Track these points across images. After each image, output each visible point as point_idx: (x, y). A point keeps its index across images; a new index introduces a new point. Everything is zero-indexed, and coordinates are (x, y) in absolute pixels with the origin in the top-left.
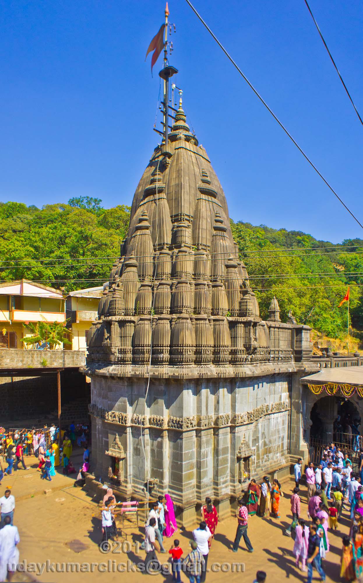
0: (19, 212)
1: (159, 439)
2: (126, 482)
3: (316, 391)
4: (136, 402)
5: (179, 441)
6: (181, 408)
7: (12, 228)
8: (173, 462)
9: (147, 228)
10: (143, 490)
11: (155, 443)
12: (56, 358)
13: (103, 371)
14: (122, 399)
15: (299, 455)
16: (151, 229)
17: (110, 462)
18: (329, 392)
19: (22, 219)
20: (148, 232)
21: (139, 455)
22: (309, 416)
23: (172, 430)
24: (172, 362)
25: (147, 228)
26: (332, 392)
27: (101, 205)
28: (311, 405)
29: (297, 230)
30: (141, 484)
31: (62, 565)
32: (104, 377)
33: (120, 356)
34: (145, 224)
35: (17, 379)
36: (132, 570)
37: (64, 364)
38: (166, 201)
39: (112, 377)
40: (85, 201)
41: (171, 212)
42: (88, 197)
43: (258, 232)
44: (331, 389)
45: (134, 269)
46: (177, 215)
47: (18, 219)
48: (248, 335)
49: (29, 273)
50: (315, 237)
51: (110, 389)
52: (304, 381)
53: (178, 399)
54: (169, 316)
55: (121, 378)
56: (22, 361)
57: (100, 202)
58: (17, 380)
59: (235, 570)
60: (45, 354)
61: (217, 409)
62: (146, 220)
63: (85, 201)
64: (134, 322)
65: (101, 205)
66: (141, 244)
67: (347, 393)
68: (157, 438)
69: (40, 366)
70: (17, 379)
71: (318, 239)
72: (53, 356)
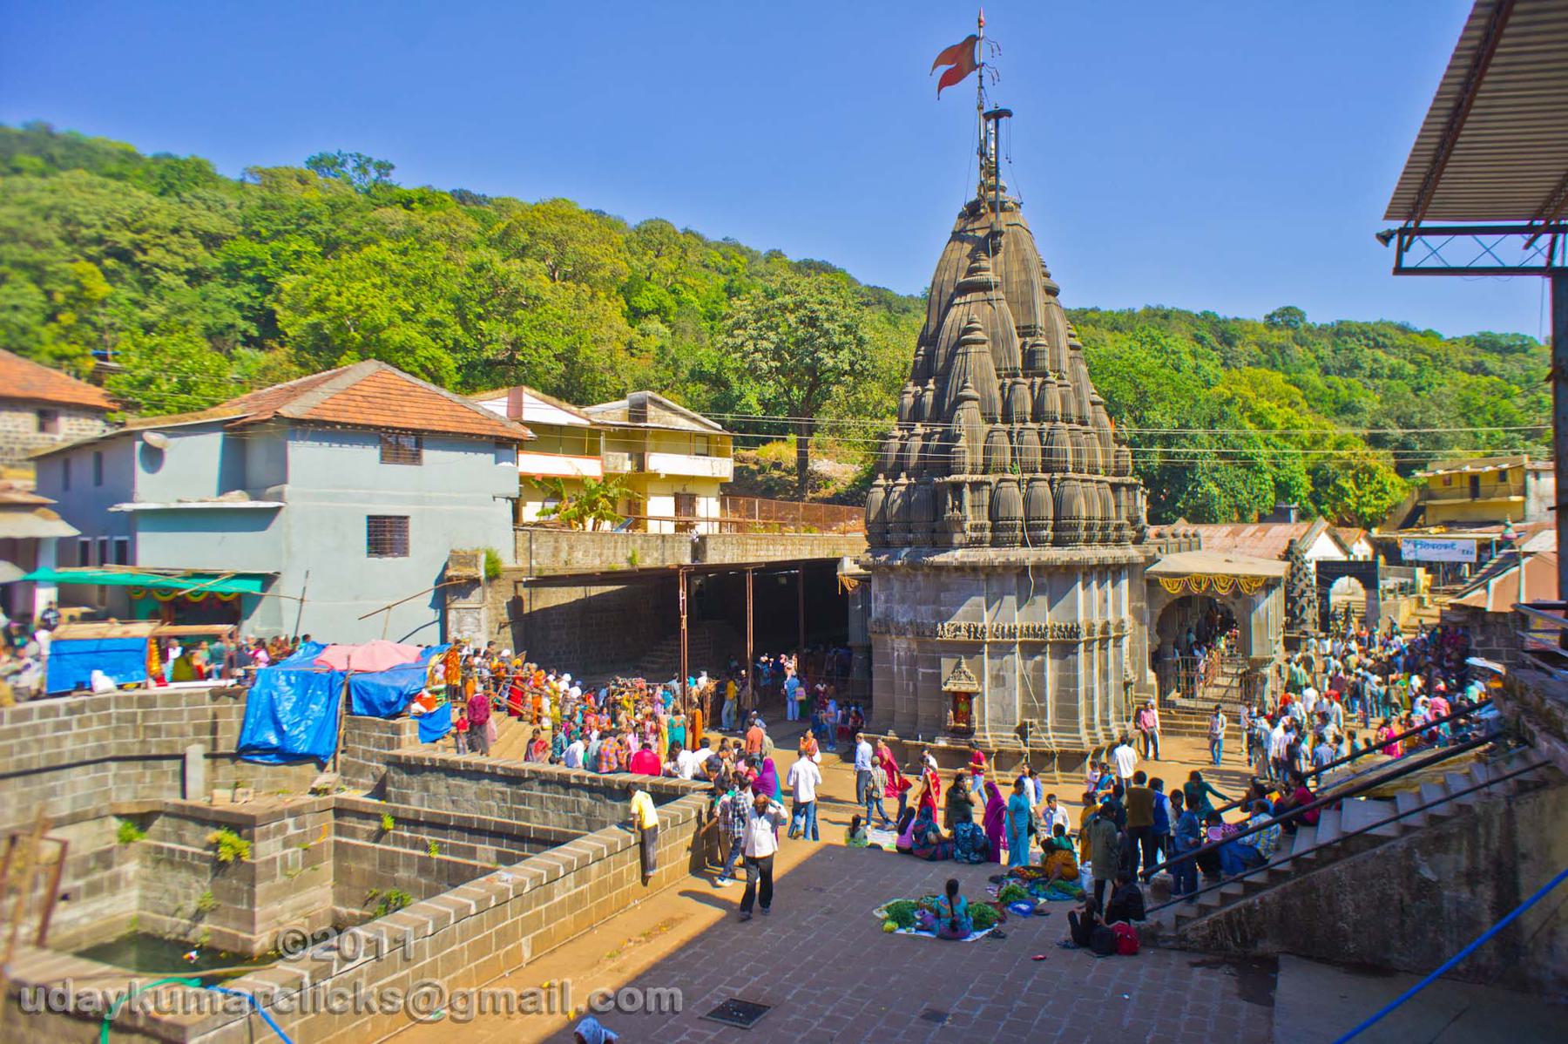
0: (196, 184)
1: (1038, 658)
2: (984, 730)
3: (1174, 589)
4: (997, 604)
5: (1070, 657)
6: (1073, 608)
7: (191, 225)
8: (1059, 691)
9: (983, 342)
10: (1015, 738)
11: (1030, 664)
12: (648, 548)
13: (940, 558)
14: (975, 599)
15: (1145, 691)
16: (990, 344)
17: (950, 703)
18: (1195, 590)
19: (210, 203)
20: (985, 347)
21: (1004, 685)
22: (1155, 628)
23: (1058, 643)
24: (1057, 542)
25: (983, 342)
26: (1199, 588)
27: (394, 178)
28: (1159, 611)
29: (818, 258)
30: (1008, 731)
31: (172, 995)
32: (940, 569)
33: (974, 534)
34: (978, 335)
35: (595, 591)
36: (367, 1005)
37: (663, 561)
38: (1004, 304)
39: (961, 568)
40: (351, 164)
41: (1017, 321)
42: (359, 156)
43: (734, 257)
44: (1199, 584)
45: (975, 404)
46: (1029, 327)
47: (198, 203)
48: (1132, 502)
49: (410, 360)
50: (860, 280)
51: (945, 588)
52: (1151, 573)
53: (1068, 596)
54: (1046, 476)
55: (974, 568)
56: (600, 555)
57: (391, 172)
58: (593, 594)
59: (193, 1006)
60: (634, 542)
61: (1103, 611)
62: (979, 330)
63: (351, 164)
64: (990, 484)
65: (394, 178)
66: (981, 367)
67: (1223, 588)
68: (1034, 656)
69: (625, 566)
70: (595, 591)
71: (864, 283)
72: (645, 546)
